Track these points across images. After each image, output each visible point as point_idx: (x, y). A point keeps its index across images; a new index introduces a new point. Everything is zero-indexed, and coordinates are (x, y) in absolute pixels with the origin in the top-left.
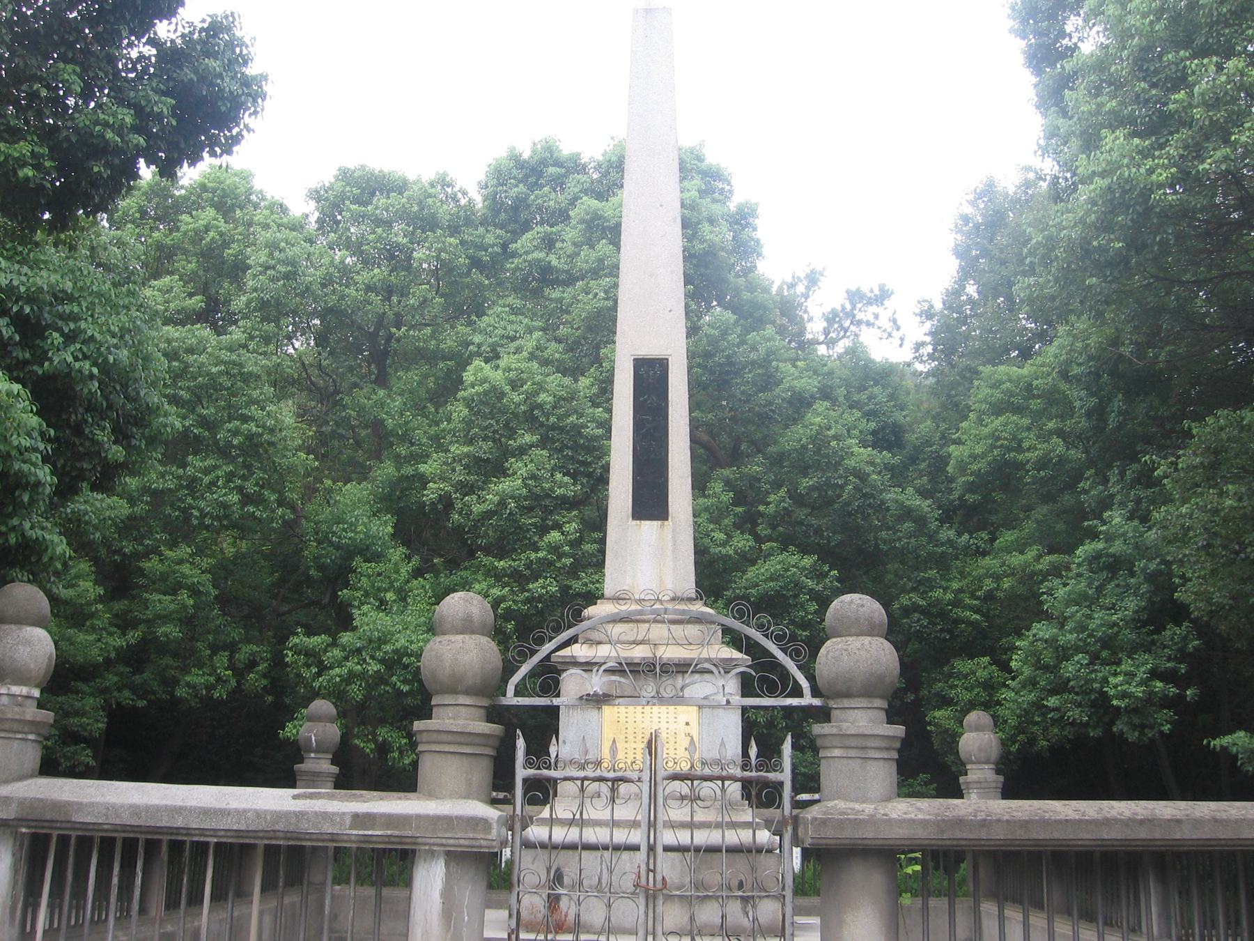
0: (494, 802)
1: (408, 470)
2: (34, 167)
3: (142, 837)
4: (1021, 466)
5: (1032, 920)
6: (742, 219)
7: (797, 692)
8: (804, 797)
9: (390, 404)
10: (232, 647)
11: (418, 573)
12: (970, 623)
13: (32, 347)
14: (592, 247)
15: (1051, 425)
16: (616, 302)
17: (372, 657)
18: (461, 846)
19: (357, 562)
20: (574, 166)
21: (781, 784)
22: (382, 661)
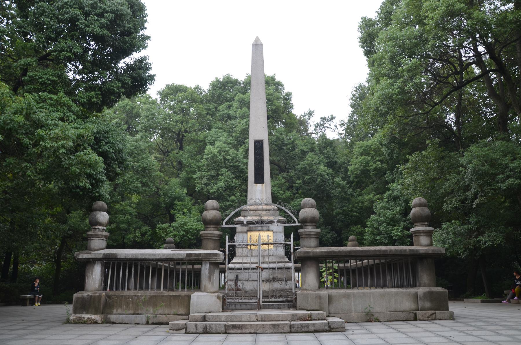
1: (190, 176)
2: (96, 98)
4: (369, 170)
6: (287, 98)
8: (297, 247)
9: (185, 157)
10: (140, 228)
11: (193, 205)
12: (355, 216)
13: (98, 145)
14: (241, 109)
15: (377, 158)
16: (249, 125)
17: (182, 230)
19: (176, 202)
20: (236, 82)
22: (184, 231)
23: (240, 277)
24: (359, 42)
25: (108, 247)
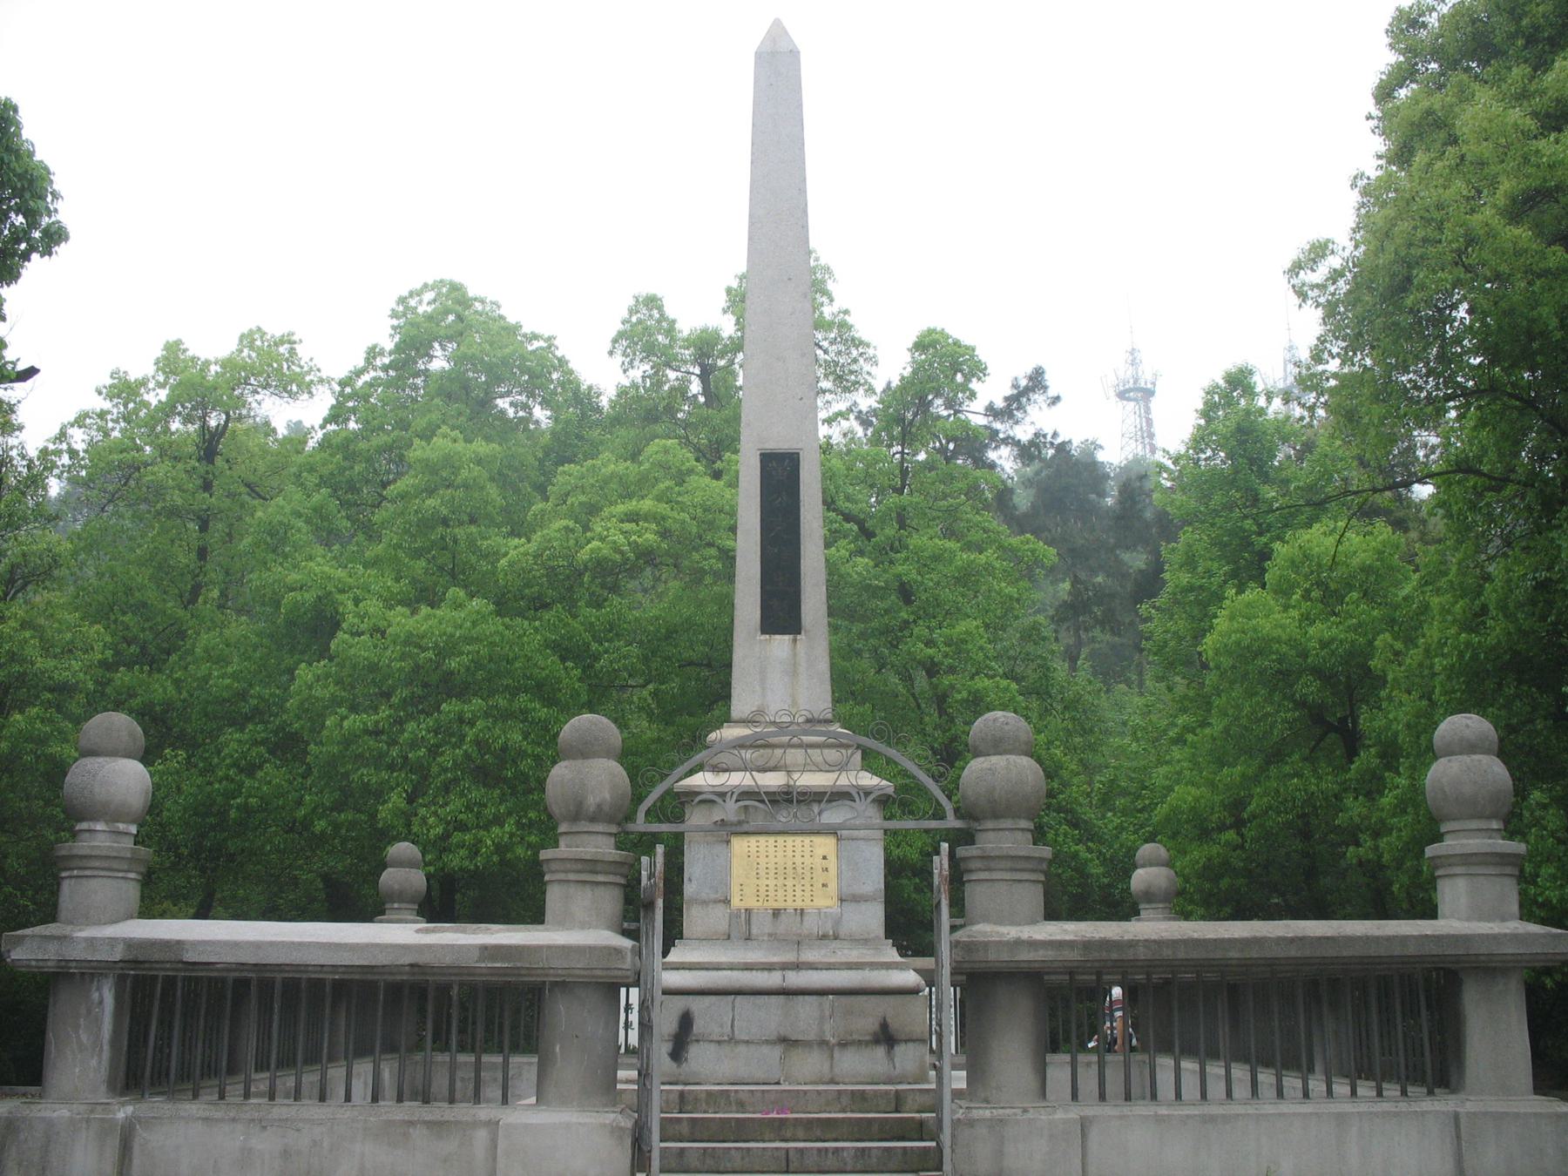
0: (625, 933)
3: (279, 976)
5: (1261, 1077)
7: (939, 815)
18: (347, 1044)
21: (1429, 911)
23: (698, 1027)
24: (645, 333)
25: (148, 910)
